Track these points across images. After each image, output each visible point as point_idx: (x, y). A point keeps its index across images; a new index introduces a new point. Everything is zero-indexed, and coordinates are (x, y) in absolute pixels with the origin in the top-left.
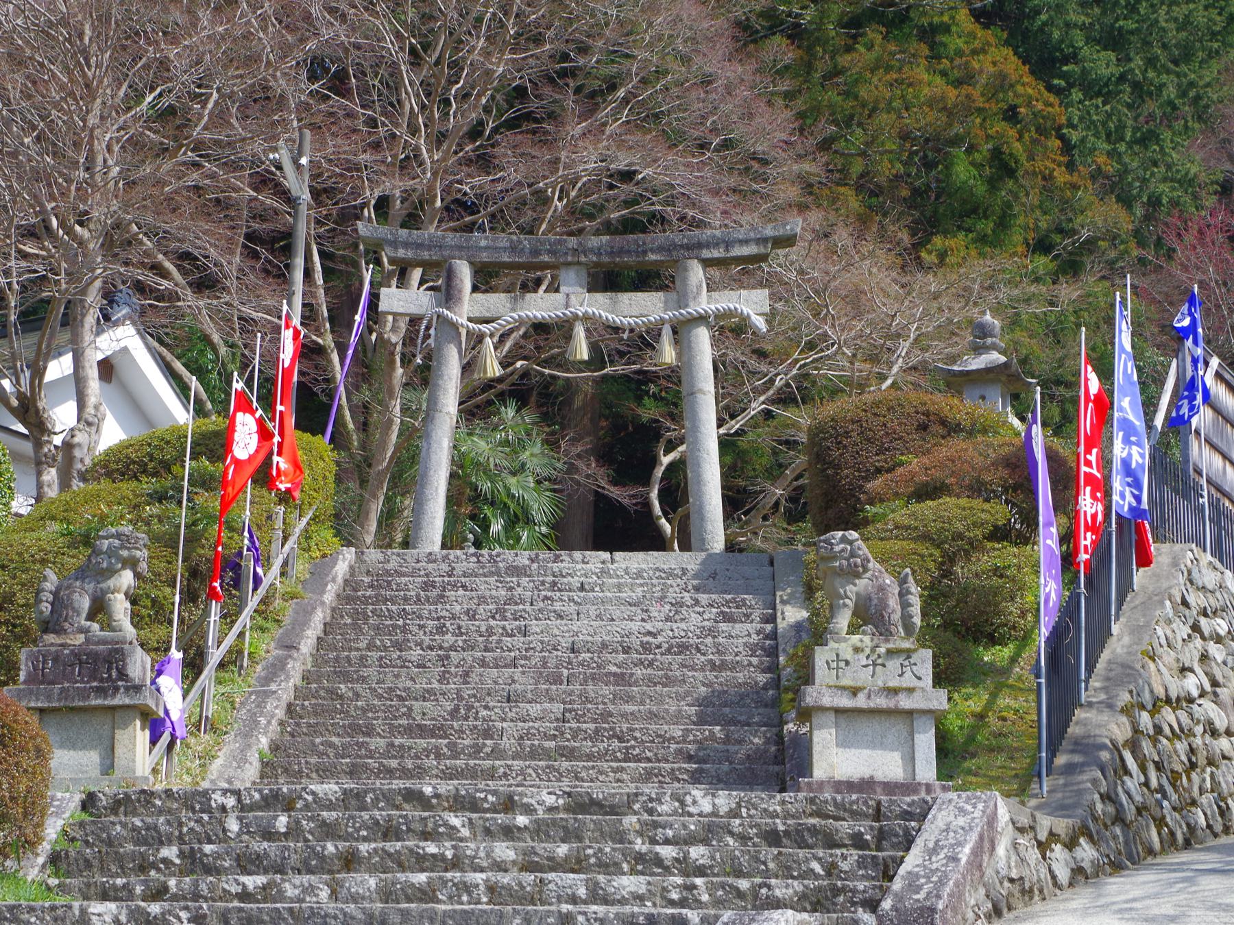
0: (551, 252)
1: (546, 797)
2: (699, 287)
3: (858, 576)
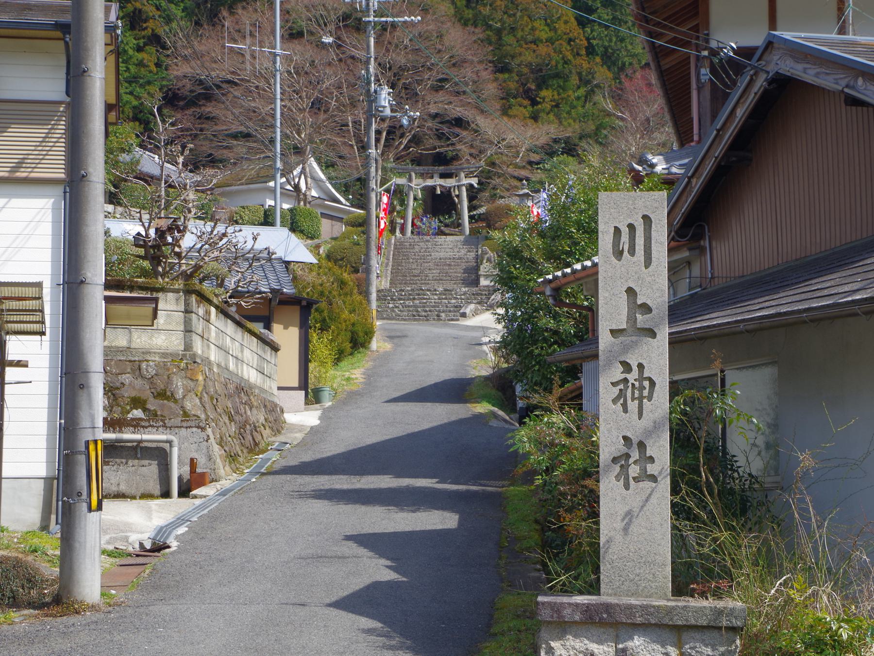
1: (441, 289)
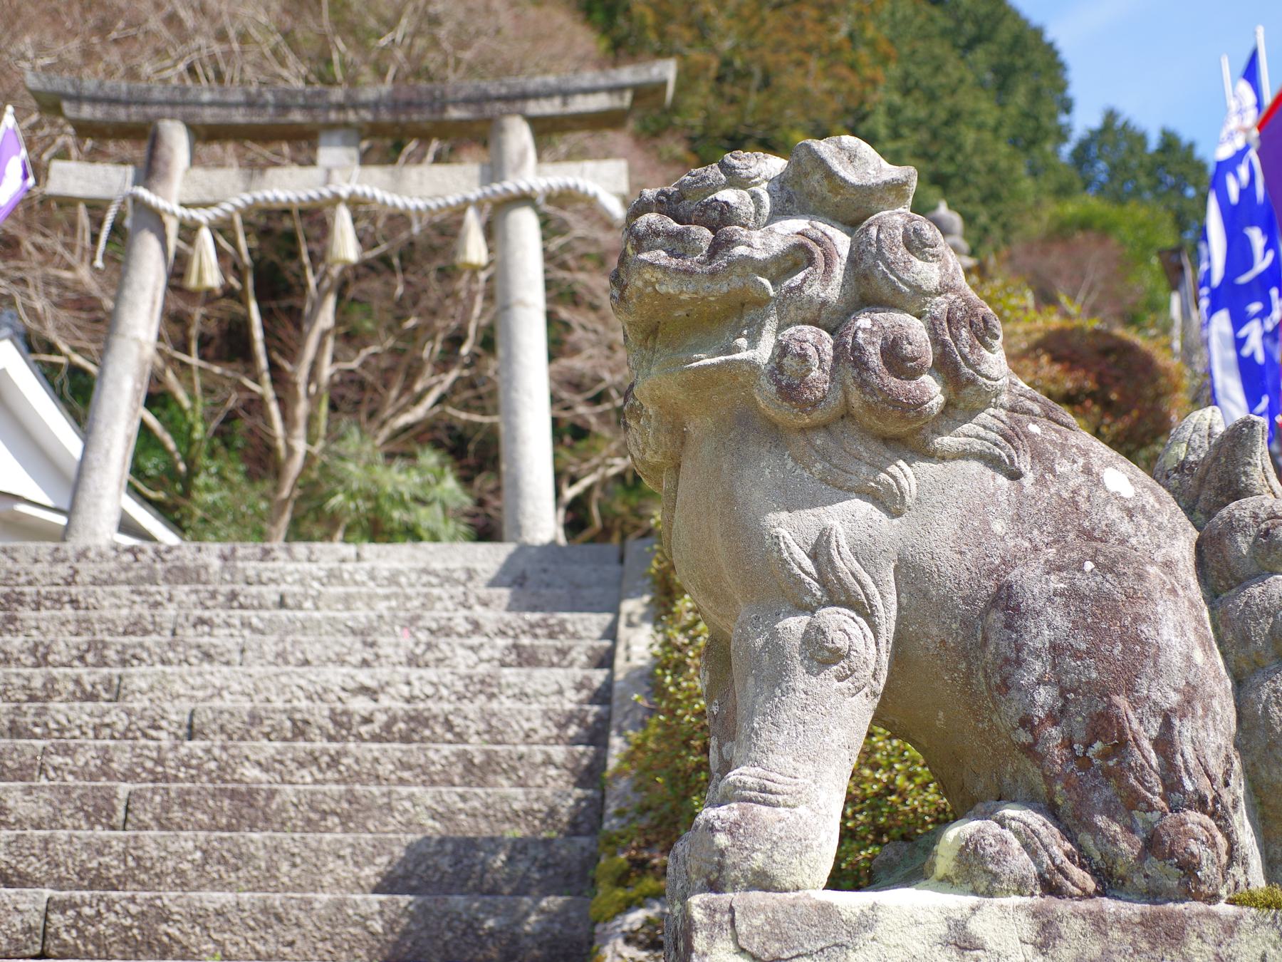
0: (307, 107)
2: (523, 155)
3: (909, 436)
